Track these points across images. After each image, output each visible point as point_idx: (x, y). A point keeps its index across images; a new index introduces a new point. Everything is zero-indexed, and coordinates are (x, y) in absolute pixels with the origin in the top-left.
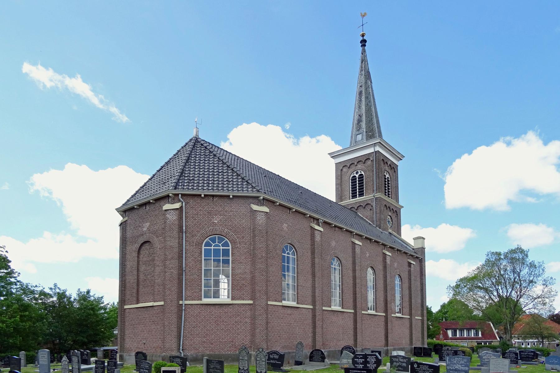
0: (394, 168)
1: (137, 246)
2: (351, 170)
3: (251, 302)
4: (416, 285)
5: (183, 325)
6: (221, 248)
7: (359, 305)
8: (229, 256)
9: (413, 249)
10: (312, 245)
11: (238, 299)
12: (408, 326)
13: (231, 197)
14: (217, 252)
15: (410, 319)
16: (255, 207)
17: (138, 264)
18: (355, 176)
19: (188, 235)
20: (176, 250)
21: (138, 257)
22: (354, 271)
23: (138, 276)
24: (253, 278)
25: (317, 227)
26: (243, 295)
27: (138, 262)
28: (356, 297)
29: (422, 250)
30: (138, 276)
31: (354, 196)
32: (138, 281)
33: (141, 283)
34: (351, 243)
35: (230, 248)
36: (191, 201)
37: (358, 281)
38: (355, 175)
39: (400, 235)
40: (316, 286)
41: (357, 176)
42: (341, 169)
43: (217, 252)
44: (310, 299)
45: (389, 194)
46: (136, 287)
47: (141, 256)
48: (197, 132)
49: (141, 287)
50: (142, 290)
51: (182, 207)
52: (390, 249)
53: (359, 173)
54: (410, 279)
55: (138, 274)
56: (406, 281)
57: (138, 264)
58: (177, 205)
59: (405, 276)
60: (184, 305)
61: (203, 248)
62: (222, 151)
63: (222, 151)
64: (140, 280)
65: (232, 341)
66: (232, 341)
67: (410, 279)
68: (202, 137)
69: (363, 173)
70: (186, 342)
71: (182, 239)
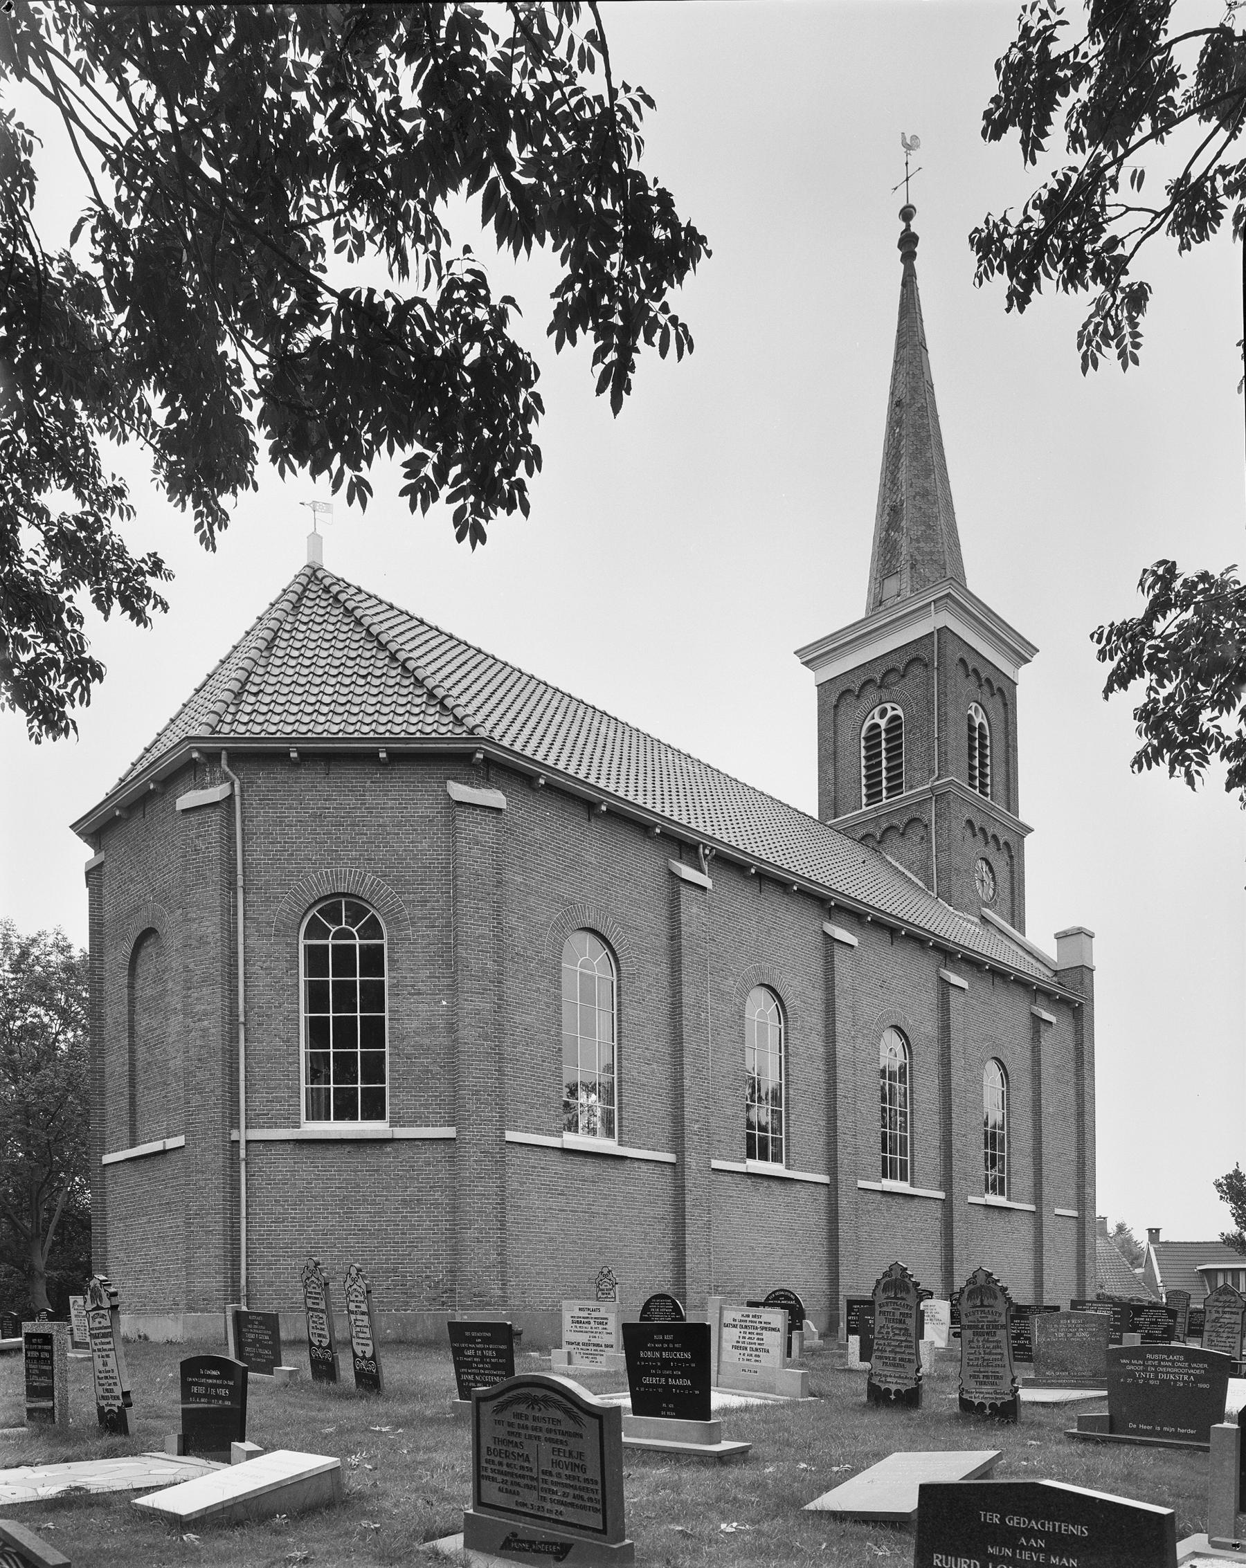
0: (1002, 694)
1: (127, 947)
2: (865, 703)
3: (449, 1132)
4: (1056, 1098)
5: (244, 1214)
6: (358, 942)
7: (843, 1158)
8: (309, 949)
9: (1056, 973)
10: (672, 938)
11: (412, 1123)
12: (1030, 1239)
13: (383, 755)
14: (344, 954)
15: (1037, 1216)
16: (460, 791)
17: (132, 1012)
18: (877, 726)
19: (251, 897)
20: (215, 950)
21: (131, 986)
22: (830, 1037)
23: (132, 1051)
24: (453, 1049)
25: (688, 872)
26: (426, 1106)
27: (132, 1002)
28: (835, 1129)
29: (1083, 973)
30: (132, 1051)
31: (874, 796)
32: (132, 1065)
33: (141, 1076)
34: (820, 938)
35: (385, 942)
36: (263, 779)
37: (841, 1072)
38: (877, 720)
39: (1022, 930)
40: (687, 1082)
41: (883, 723)
42: (837, 700)
43: (344, 954)
44: (664, 1129)
45: (983, 785)
46: (126, 1091)
47: (139, 983)
48: (315, 540)
49: (140, 1088)
50: (145, 1099)
51: (230, 798)
52: (963, 966)
53: (890, 713)
54: (1037, 1077)
55: (132, 1044)
56: (1022, 1080)
57: (132, 1012)
58: (216, 793)
59: (1019, 1061)
60: (243, 1145)
61: (302, 943)
62: (574, 704)
63: (574, 704)
64: (139, 1065)
65: (395, 1270)
66: (395, 1270)
67: (1037, 1077)
68: (334, 565)
69: (900, 712)
70: (256, 1272)
71: (236, 914)
